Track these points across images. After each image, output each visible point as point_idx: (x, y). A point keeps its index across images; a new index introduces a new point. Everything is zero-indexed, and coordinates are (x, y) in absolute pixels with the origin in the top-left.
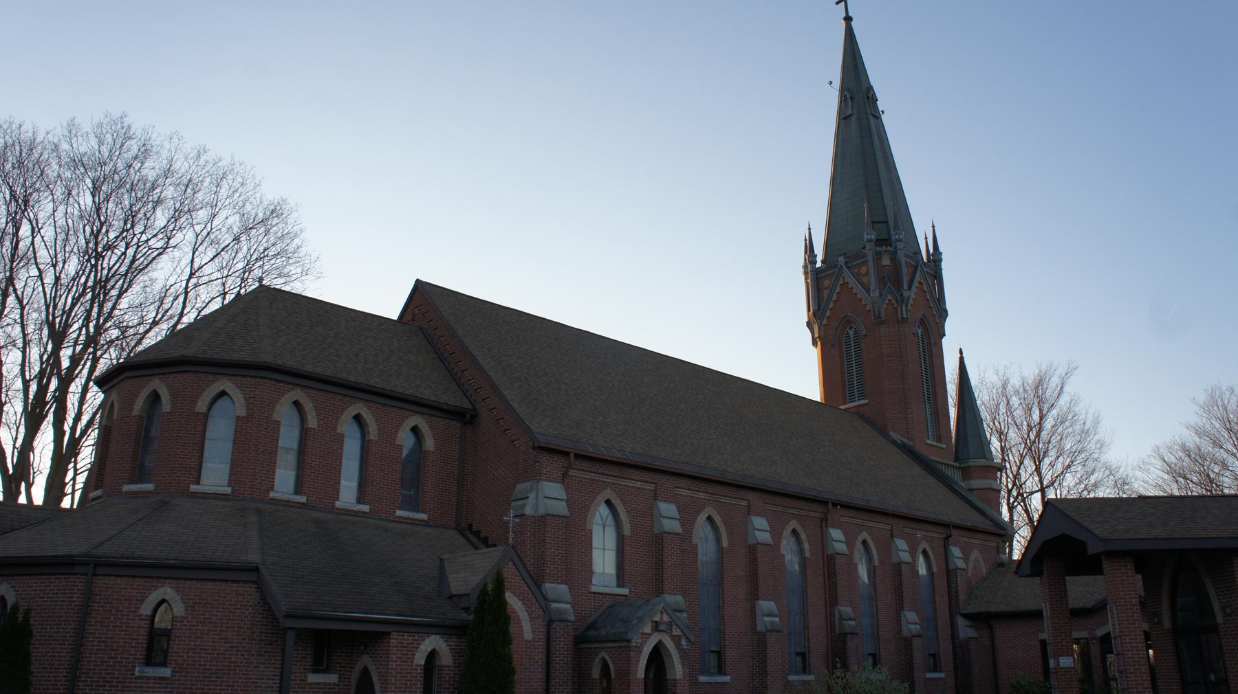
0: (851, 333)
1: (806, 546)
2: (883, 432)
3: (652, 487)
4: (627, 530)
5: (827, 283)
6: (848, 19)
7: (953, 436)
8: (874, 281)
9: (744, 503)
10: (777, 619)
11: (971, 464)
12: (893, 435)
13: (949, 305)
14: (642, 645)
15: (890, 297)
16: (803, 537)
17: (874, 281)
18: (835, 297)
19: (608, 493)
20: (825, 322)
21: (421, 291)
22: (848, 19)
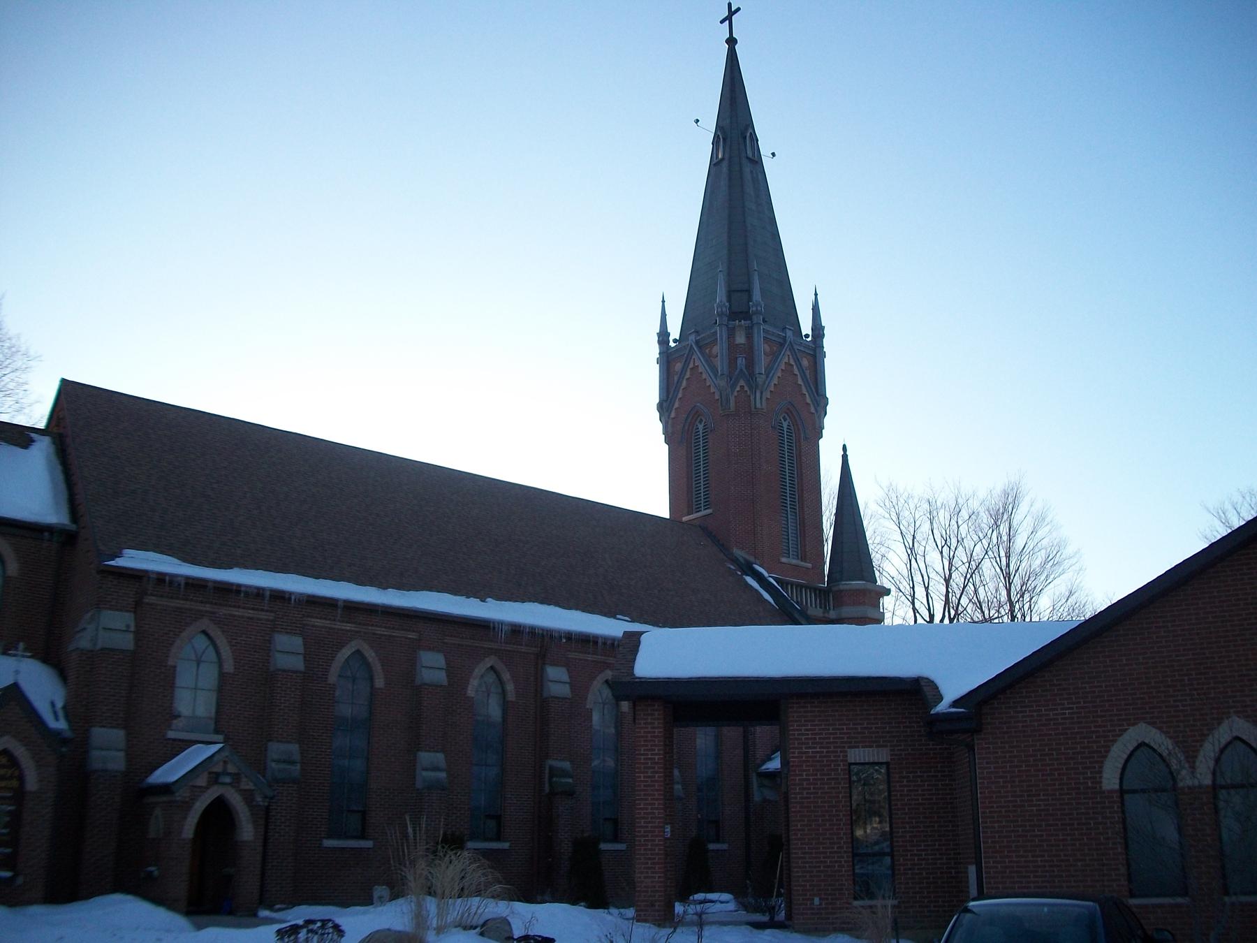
0: (701, 427)
1: (510, 687)
2: (724, 548)
3: (271, 616)
4: (229, 667)
5: (678, 367)
6: (732, 41)
7: (828, 548)
8: (743, 363)
9: (412, 636)
10: (443, 775)
11: (841, 587)
12: (738, 552)
13: (830, 392)
14: (193, 799)
15: (742, 383)
16: (506, 676)
17: (743, 363)
18: (684, 383)
19: (205, 623)
20: (673, 415)
21: (71, 394)
22: (732, 41)
